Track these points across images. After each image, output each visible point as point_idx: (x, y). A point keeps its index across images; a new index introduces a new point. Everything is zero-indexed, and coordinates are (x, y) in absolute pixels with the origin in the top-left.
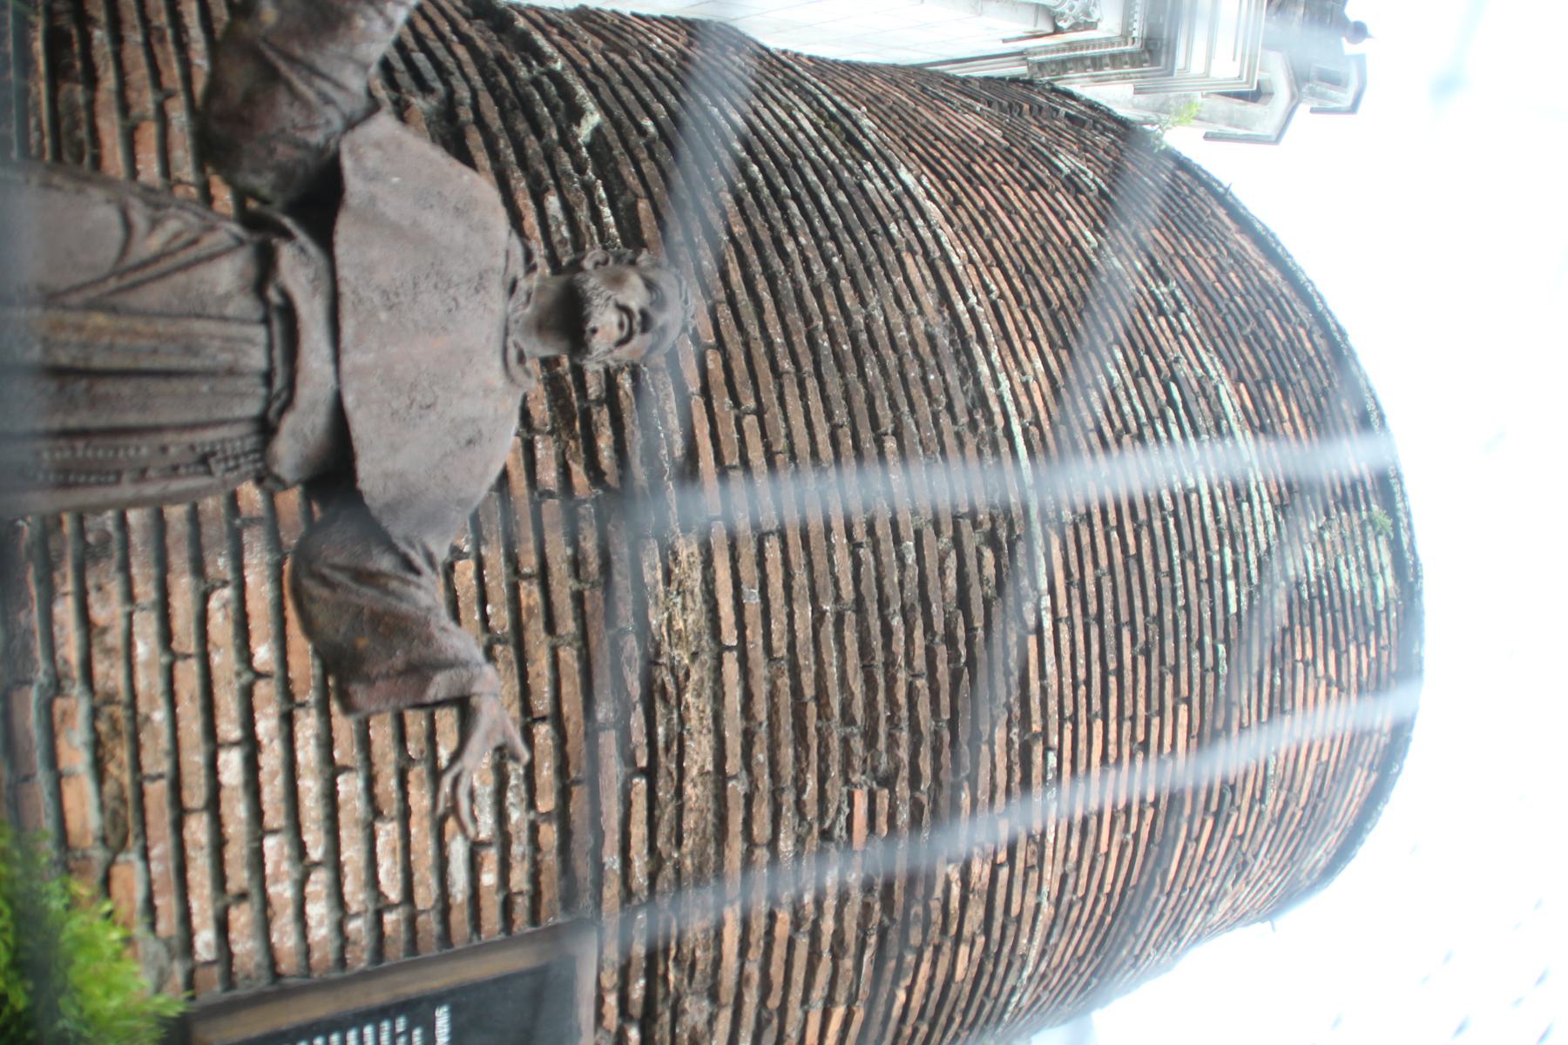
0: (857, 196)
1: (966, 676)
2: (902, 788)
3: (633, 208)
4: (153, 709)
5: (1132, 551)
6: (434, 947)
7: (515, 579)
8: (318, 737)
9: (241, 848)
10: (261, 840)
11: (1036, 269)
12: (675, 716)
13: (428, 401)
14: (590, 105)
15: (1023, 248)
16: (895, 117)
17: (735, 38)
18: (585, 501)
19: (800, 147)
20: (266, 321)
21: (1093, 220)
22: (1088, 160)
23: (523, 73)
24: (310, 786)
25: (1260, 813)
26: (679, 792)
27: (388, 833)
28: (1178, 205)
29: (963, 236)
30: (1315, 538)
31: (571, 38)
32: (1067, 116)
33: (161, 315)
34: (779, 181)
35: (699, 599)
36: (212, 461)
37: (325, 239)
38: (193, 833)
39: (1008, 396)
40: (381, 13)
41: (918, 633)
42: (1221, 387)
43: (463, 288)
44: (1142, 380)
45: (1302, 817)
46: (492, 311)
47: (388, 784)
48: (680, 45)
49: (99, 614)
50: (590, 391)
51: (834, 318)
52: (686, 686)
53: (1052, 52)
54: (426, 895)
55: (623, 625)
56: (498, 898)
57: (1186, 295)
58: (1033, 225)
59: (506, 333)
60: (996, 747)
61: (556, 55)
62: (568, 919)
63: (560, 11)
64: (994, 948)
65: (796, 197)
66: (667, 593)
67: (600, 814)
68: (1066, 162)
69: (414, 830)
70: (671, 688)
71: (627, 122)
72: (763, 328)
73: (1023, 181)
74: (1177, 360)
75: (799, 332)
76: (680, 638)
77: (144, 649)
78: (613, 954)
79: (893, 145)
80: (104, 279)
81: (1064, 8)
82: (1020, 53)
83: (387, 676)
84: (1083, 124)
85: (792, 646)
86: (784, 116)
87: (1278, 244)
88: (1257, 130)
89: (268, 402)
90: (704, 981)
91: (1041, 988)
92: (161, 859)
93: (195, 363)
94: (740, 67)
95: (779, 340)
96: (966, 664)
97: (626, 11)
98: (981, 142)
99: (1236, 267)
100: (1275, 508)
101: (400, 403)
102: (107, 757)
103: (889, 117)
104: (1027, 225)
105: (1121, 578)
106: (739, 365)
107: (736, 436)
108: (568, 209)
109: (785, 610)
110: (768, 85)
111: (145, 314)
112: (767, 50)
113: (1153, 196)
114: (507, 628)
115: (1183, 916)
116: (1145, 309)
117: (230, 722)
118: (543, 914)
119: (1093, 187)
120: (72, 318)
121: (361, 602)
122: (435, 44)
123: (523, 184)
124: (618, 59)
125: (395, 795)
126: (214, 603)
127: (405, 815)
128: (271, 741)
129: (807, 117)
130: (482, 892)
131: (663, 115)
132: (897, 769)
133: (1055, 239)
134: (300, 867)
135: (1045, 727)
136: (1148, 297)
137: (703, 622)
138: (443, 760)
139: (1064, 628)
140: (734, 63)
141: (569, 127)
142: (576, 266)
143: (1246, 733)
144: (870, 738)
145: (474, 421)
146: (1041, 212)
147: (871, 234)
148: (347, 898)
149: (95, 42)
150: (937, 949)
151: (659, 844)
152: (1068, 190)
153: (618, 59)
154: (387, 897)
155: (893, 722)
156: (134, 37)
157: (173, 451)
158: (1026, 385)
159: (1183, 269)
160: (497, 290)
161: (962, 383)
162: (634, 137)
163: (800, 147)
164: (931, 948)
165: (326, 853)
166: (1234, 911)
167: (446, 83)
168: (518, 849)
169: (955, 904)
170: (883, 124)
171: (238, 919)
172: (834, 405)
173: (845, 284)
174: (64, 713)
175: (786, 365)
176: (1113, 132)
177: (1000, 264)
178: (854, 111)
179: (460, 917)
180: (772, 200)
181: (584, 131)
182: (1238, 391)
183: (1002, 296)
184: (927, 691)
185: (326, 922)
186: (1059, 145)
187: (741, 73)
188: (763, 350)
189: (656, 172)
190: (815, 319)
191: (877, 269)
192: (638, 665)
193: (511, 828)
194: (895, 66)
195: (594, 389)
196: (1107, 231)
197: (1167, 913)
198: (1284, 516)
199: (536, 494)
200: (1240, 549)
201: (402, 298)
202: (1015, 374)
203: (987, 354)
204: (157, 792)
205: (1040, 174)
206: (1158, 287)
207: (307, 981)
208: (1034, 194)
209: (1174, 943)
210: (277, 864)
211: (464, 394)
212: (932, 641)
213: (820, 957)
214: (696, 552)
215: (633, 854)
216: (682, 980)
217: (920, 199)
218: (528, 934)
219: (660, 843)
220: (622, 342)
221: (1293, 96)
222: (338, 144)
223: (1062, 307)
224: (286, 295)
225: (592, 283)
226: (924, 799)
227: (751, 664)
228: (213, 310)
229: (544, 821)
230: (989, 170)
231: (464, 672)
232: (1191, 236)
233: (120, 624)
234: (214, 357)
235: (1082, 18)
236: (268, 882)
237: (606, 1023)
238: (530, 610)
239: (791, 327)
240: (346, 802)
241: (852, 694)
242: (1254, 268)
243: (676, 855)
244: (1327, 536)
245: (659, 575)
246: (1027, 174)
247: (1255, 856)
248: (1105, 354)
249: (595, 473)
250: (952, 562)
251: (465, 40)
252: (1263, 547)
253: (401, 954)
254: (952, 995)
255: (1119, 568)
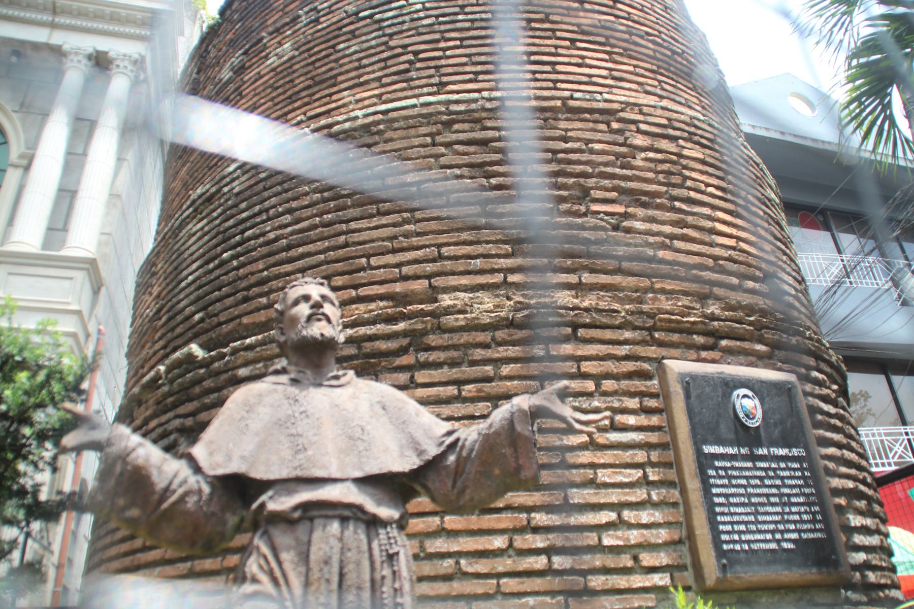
0: (242, 196)
2: (591, 182)
3: (246, 326)
5: (458, 43)
6: (669, 452)
9: (608, 558)
11: (289, 93)
13: (360, 430)
14: (185, 350)
15: (277, 100)
17: (146, 267)
18: (417, 357)
20: (311, 519)
21: (261, 59)
23: (166, 389)
28: (253, 8)
32: (198, 73)
36: (391, 552)
37: (264, 485)
38: (599, 585)
40: (134, 450)
44: (357, 33)
50: (353, 352)
51: (315, 211)
52: (526, 303)
54: (640, 456)
57: (307, 5)
58: (263, 94)
60: (569, 127)
61: (155, 369)
62: (657, 377)
63: (129, 368)
67: (597, 355)
68: (226, 74)
69: (602, 461)
73: (236, 99)
83: (517, 458)
86: (194, 239)
89: (357, 519)
91: (710, 110)
103: (196, 178)
104: (263, 98)
105: (474, 50)
106: (339, 266)
107: (382, 270)
108: (246, 364)
115: (673, 25)
116: (315, 29)
119: (241, 58)
121: (473, 471)
126: (470, 570)
127: (593, 466)
128: (548, 539)
129: (195, 225)
130: (639, 424)
131: (192, 308)
132: (580, 185)
133: (271, 82)
134: (620, 526)
135: (559, 98)
136: (307, 28)
138: (564, 426)
140: (162, 268)
141: (198, 362)
145: (372, 405)
146: (255, 89)
147: (265, 189)
150: (685, 167)
154: (639, 477)
158: (357, 101)
165: (613, 511)
169: (659, 156)
170: (200, 182)
176: (208, 46)
183: (305, 114)
186: (215, 78)
187: (168, 263)
188: (332, 253)
190: (314, 222)
191: (286, 186)
196: (268, 51)
199: (412, 385)
201: (300, 442)
203: (338, 123)
205: (232, 89)
206: (302, 22)
207: (684, 524)
208: (244, 93)
210: (618, 538)
216: (695, 314)
218: (664, 399)
220: (329, 320)
224: (296, 508)
229: (600, 388)
231: (516, 414)
236: (629, 544)
237: (717, 358)
240: (585, 499)
245: (462, 316)
246: (232, 97)
248: (340, 54)
249: (403, 351)
253: (672, 471)
254: (711, 161)
255: (468, 51)
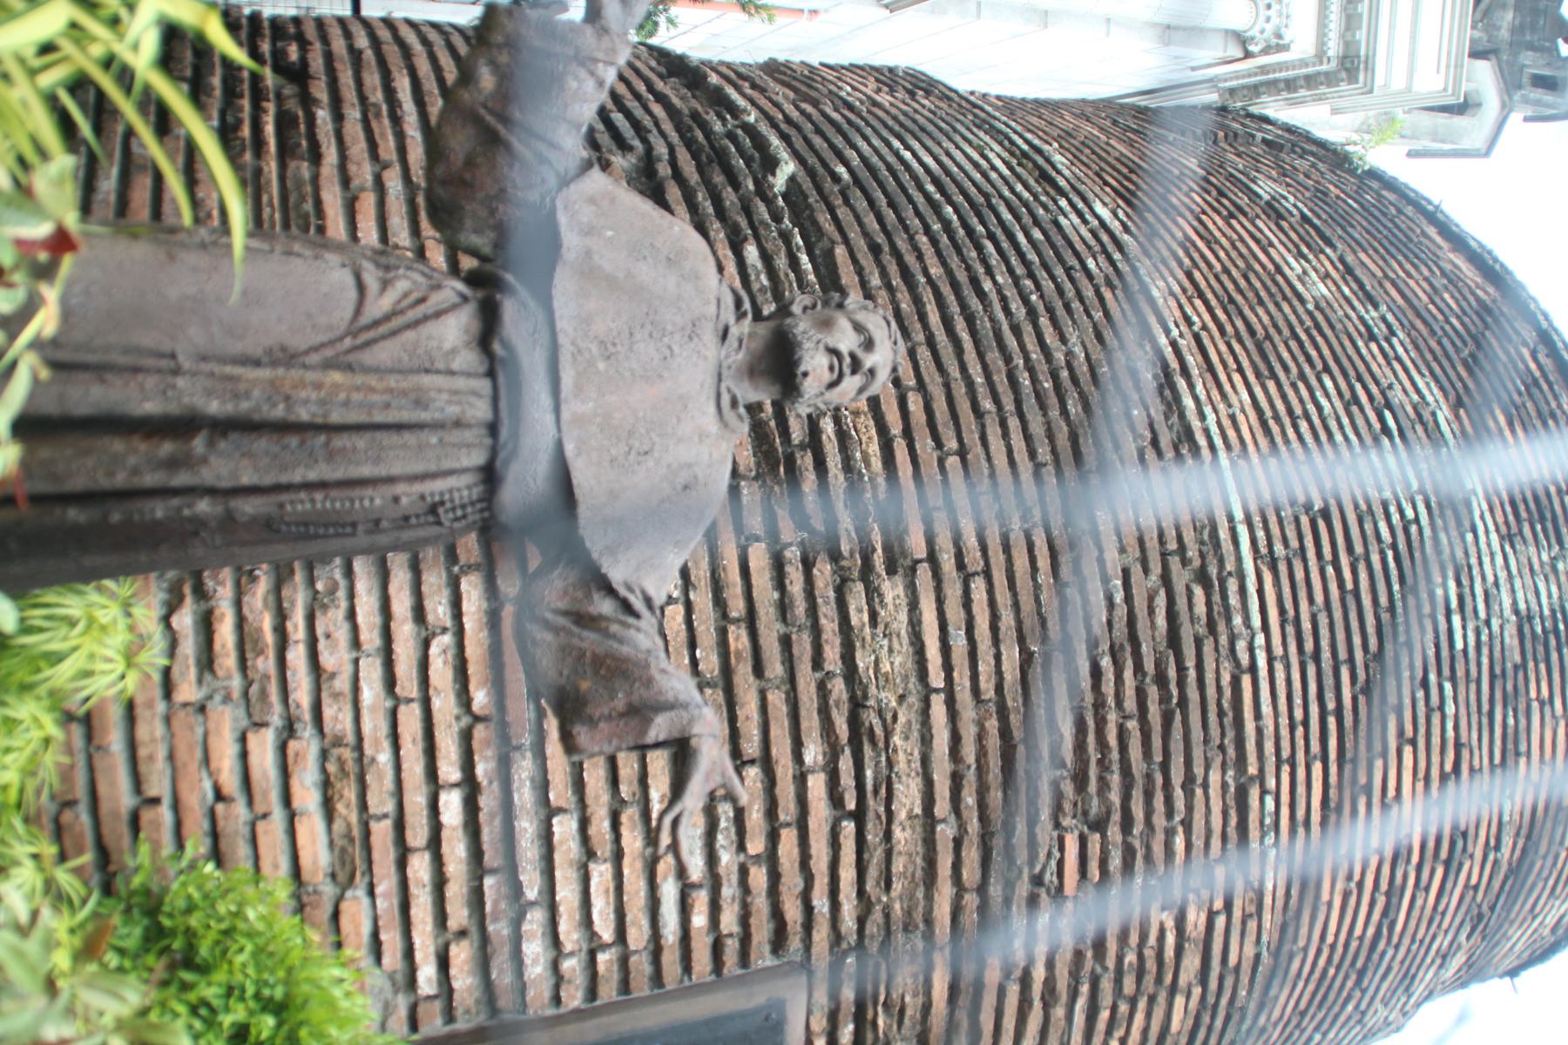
0: (1053, 232)
1: (1178, 717)
2: (1114, 832)
3: (830, 254)
4: (378, 752)
5: (1349, 586)
7: (723, 623)
8: (532, 780)
10: (481, 879)
11: (1239, 299)
12: (883, 759)
13: (645, 448)
14: (784, 155)
15: (1224, 278)
16: (1087, 151)
18: (791, 544)
19: (993, 186)
21: (1297, 246)
22: (1288, 185)
23: (718, 127)
24: (527, 827)
25: (1496, 862)
26: (888, 835)
27: (601, 875)
29: (1162, 268)
30: (1547, 568)
31: (762, 90)
32: (1264, 141)
33: (392, 371)
34: (974, 221)
35: (905, 641)
36: (441, 510)
39: (1214, 430)
41: (1128, 674)
42: (1439, 414)
43: (677, 337)
44: (1354, 409)
45: (1542, 867)
46: (706, 358)
47: (601, 826)
48: (869, 92)
49: (328, 660)
51: (1034, 356)
53: (1244, 77)
54: (638, 936)
55: (831, 668)
56: (709, 940)
58: (1234, 254)
59: (720, 380)
62: (776, 962)
64: (1211, 1000)
65: (991, 237)
66: (874, 636)
67: (810, 857)
68: (1265, 188)
69: (626, 871)
70: (879, 731)
71: (820, 170)
72: (963, 369)
74: (1390, 387)
75: (999, 372)
76: (887, 680)
77: (371, 692)
78: (822, 998)
79: (1086, 180)
80: (341, 339)
81: (1254, 32)
82: (1210, 80)
83: (609, 718)
84: (1281, 148)
85: (999, 688)
86: (976, 156)
87: (1496, 260)
88: (1465, 144)
90: (914, 1027)
92: (386, 895)
93: (425, 416)
94: (930, 111)
95: (979, 380)
96: (1178, 704)
97: (814, 61)
98: (1176, 172)
99: (1451, 287)
100: (1502, 538)
101: (618, 450)
102: (336, 797)
104: (1227, 254)
106: (940, 405)
108: (766, 257)
109: (992, 651)
110: (959, 126)
111: (376, 370)
112: (956, 92)
113: (1358, 217)
114: (716, 672)
115: (1413, 970)
116: (1355, 335)
117: (451, 764)
118: (753, 957)
119: (1295, 212)
120: (311, 376)
121: (585, 645)
122: (632, 104)
123: (722, 235)
124: (809, 108)
125: (608, 836)
126: (434, 650)
127: (618, 856)
129: (999, 156)
130: (693, 934)
131: (856, 161)
132: (1108, 813)
133: (1257, 267)
135: (1261, 770)
136: (1357, 322)
137: (910, 664)
139: (1279, 668)
141: (765, 177)
142: (784, 310)
143: (1477, 777)
144: (1080, 780)
145: (689, 466)
146: (1242, 240)
147: (1068, 271)
148: (562, 937)
149: (319, 122)
150: (1152, 999)
151: (868, 888)
152: (1269, 217)
153: (809, 108)
155: (1103, 764)
156: (353, 114)
157: (404, 501)
158: (1233, 418)
159: (1393, 292)
160: (709, 337)
161: (1167, 418)
162: (828, 184)
163: (993, 186)
164: (1145, 998)
166: (1470, 967)
167: (645, 141)
168: (729, 891)
170: (1076, 159)
171: (458, 955)
172: (1037, 444)
173: (1044, 321)
174: (297, 755)
175: (987, 404)
176: (1313, 154)
177: (1201, 296)
178: (1046, 147)
179: (670, 959)
180: (967, 241)
181: (779, 181)
182: (1457, 416)
183: (1204, 327)
184: (1138, 733)
185: (542, 960)
188: (963, 390)
189: (851, 218)
191: (1076, 305)
192: (845, 707)
193: (722, 870)
194: (1084, 101)
195: (797, 433)
196: (1311, 257)
197: (1396, 966)
198: (1513, 546)
200: (1465, 582)
201: (619, 348)
202: (1221, 407)
203: (1191, 386)
204: (382, 831)
206: (1367, 312)
208: (1233, 222)
209: (1403, 999)
210: (496, 903)
211: (680, 440)
212: (1142, 681)
213: (1031, 1005)
214: (902, 594)
215: (842, 897)
217: (1117, 233)
218: (738, 976)
219: (869, 886)
221: (1503, 105)
222: (553, 201)
223: (1268, 337)
225: (802, 327)
226: (1137, 844)
227: (958, 706)
228: (440, 365)
230: (1186, 200)
231: (684, 714)
232: (1400, 258)
233: (348, 670)
234: (442, 410)
235: (1274, 41)
238: (738, 654)
239: (991, 367)
240: (561, 843)
241: (1062, 736)
242: (1469, 288)
243: (885, 899)
244: (1560, 566)
245: (866, 617)
247: (1492, 908)
250: (1161, 601)
251: (661, 98)
252: (1490, 579)
